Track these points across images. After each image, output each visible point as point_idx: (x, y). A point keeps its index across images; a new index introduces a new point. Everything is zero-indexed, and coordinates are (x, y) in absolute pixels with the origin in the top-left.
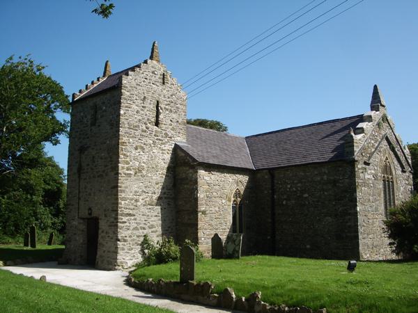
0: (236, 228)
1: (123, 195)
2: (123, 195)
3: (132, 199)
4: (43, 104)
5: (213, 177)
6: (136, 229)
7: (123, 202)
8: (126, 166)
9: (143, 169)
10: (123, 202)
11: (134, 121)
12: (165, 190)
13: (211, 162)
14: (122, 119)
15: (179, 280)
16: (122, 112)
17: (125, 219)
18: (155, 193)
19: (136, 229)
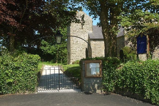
0: (74, 68)
1: (72, 49)
2: (72, 49)
3: (75, 49)
4: (132, 71)
5: (96, 42)
6: (76, 57)
7: (72, 50)
8: (73, 41)
9: (78, 42)
10: (72, 50)
11: (75, 29)
12: (63, 31)
13: (95, 38)
14: (71, 30)
15: (103, 42)
16: (71, 28)
17: (72, 54)
18: (82, 47)
19: (76, 57)
